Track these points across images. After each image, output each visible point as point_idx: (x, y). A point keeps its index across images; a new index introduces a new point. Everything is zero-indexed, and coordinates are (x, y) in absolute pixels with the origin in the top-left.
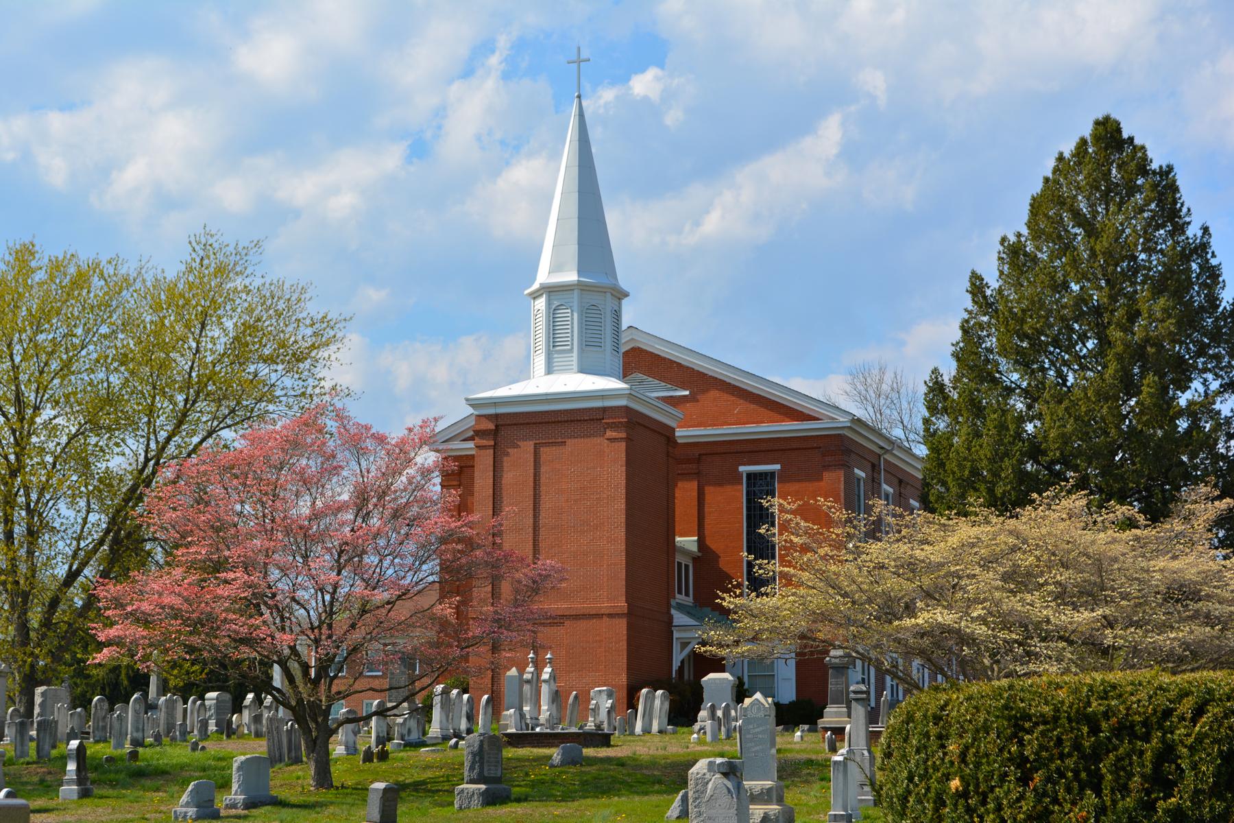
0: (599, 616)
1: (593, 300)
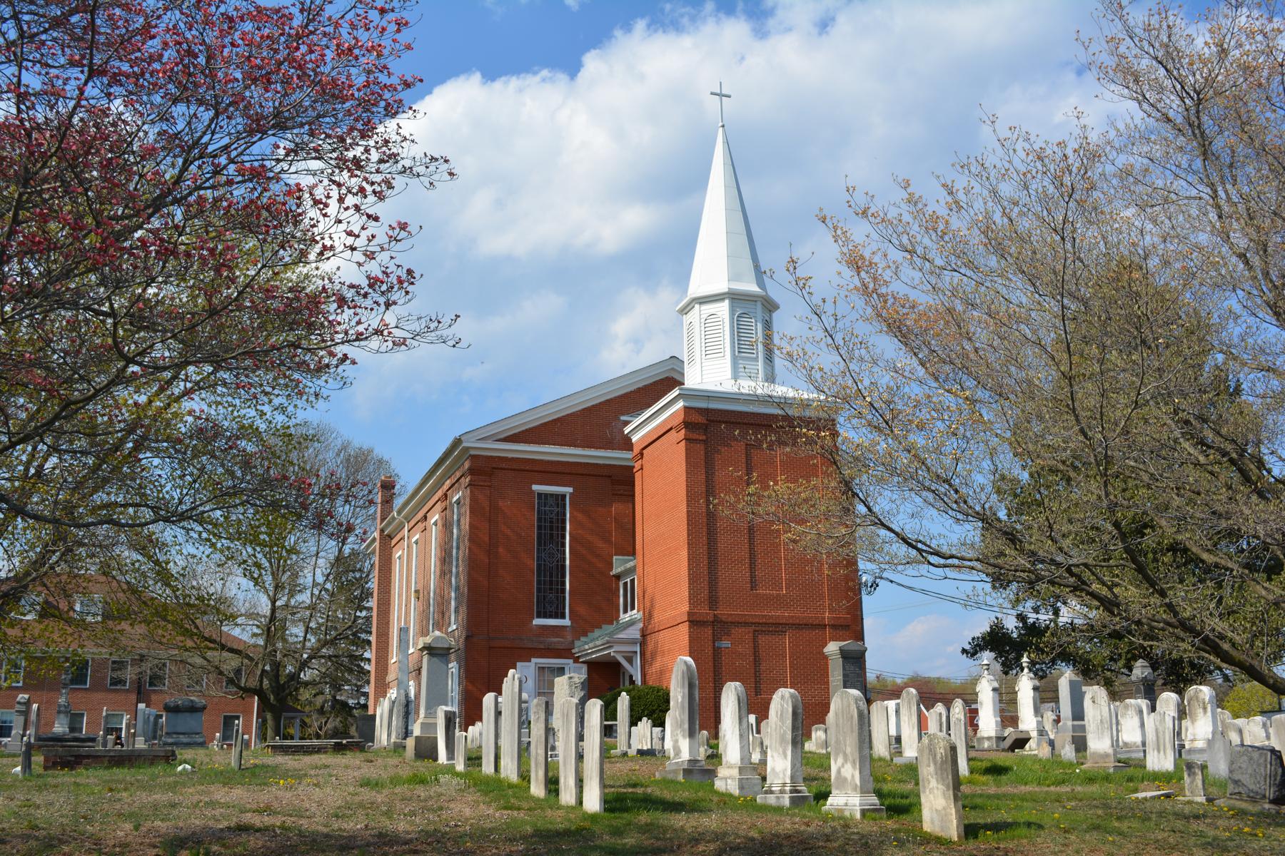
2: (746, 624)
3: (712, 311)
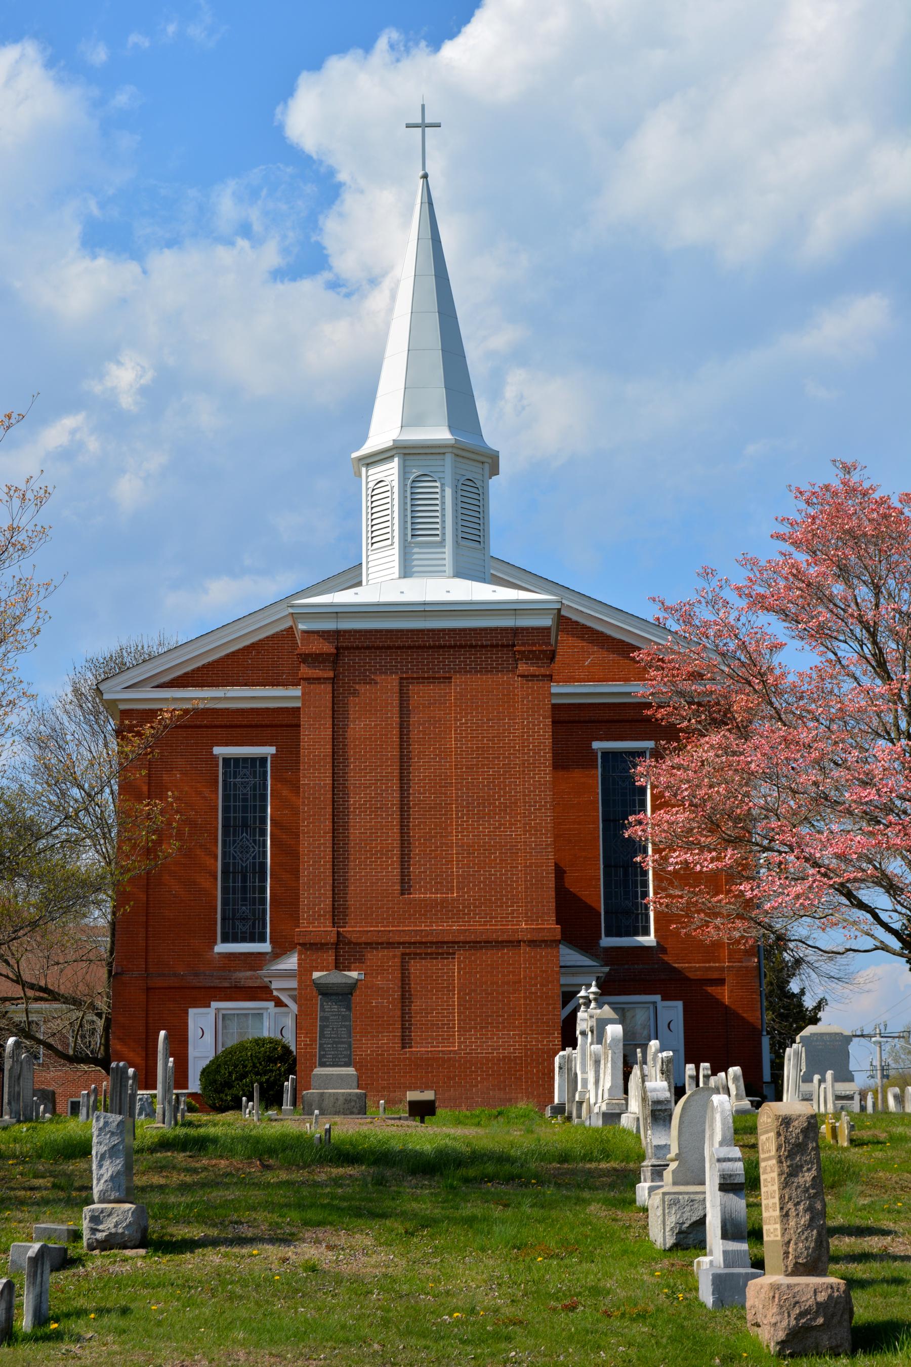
0: (515, 944)
1: (457, 476)
2: (390, 945)
3: (379, 477)
